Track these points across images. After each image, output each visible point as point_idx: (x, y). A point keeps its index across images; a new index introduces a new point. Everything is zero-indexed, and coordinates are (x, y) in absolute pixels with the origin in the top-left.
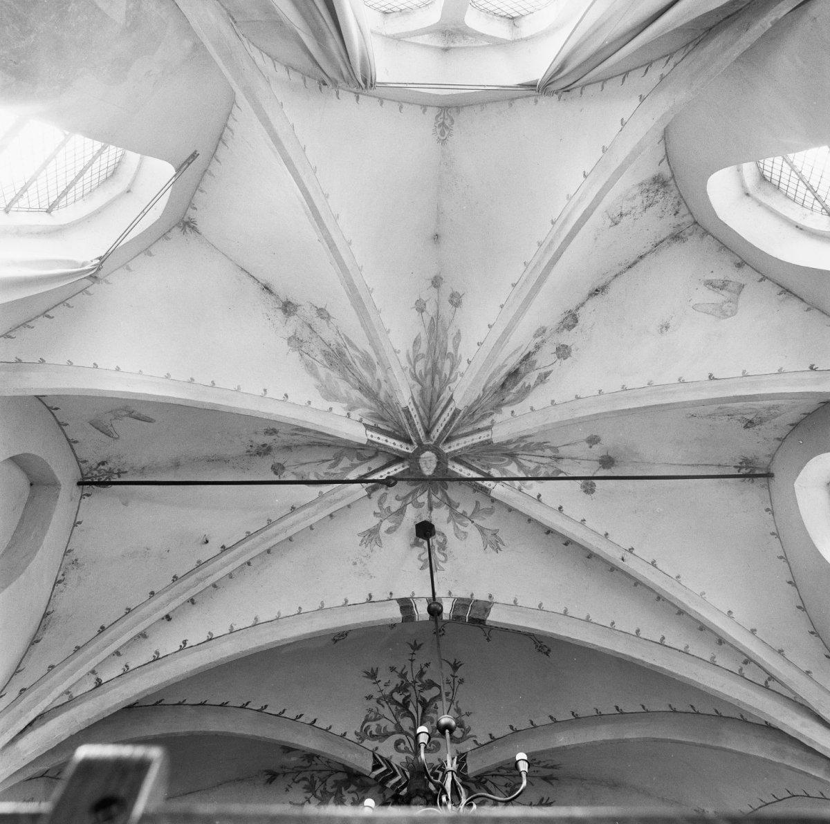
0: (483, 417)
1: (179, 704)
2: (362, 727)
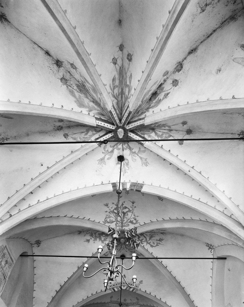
0: (142, 113)
1: (43, 218)
2: (105, 220)
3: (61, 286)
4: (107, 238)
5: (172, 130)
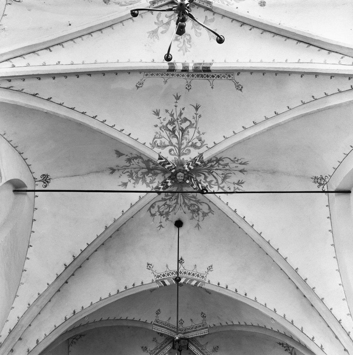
2: (153, 141)
3: (73, 256)
4: (155, 179)
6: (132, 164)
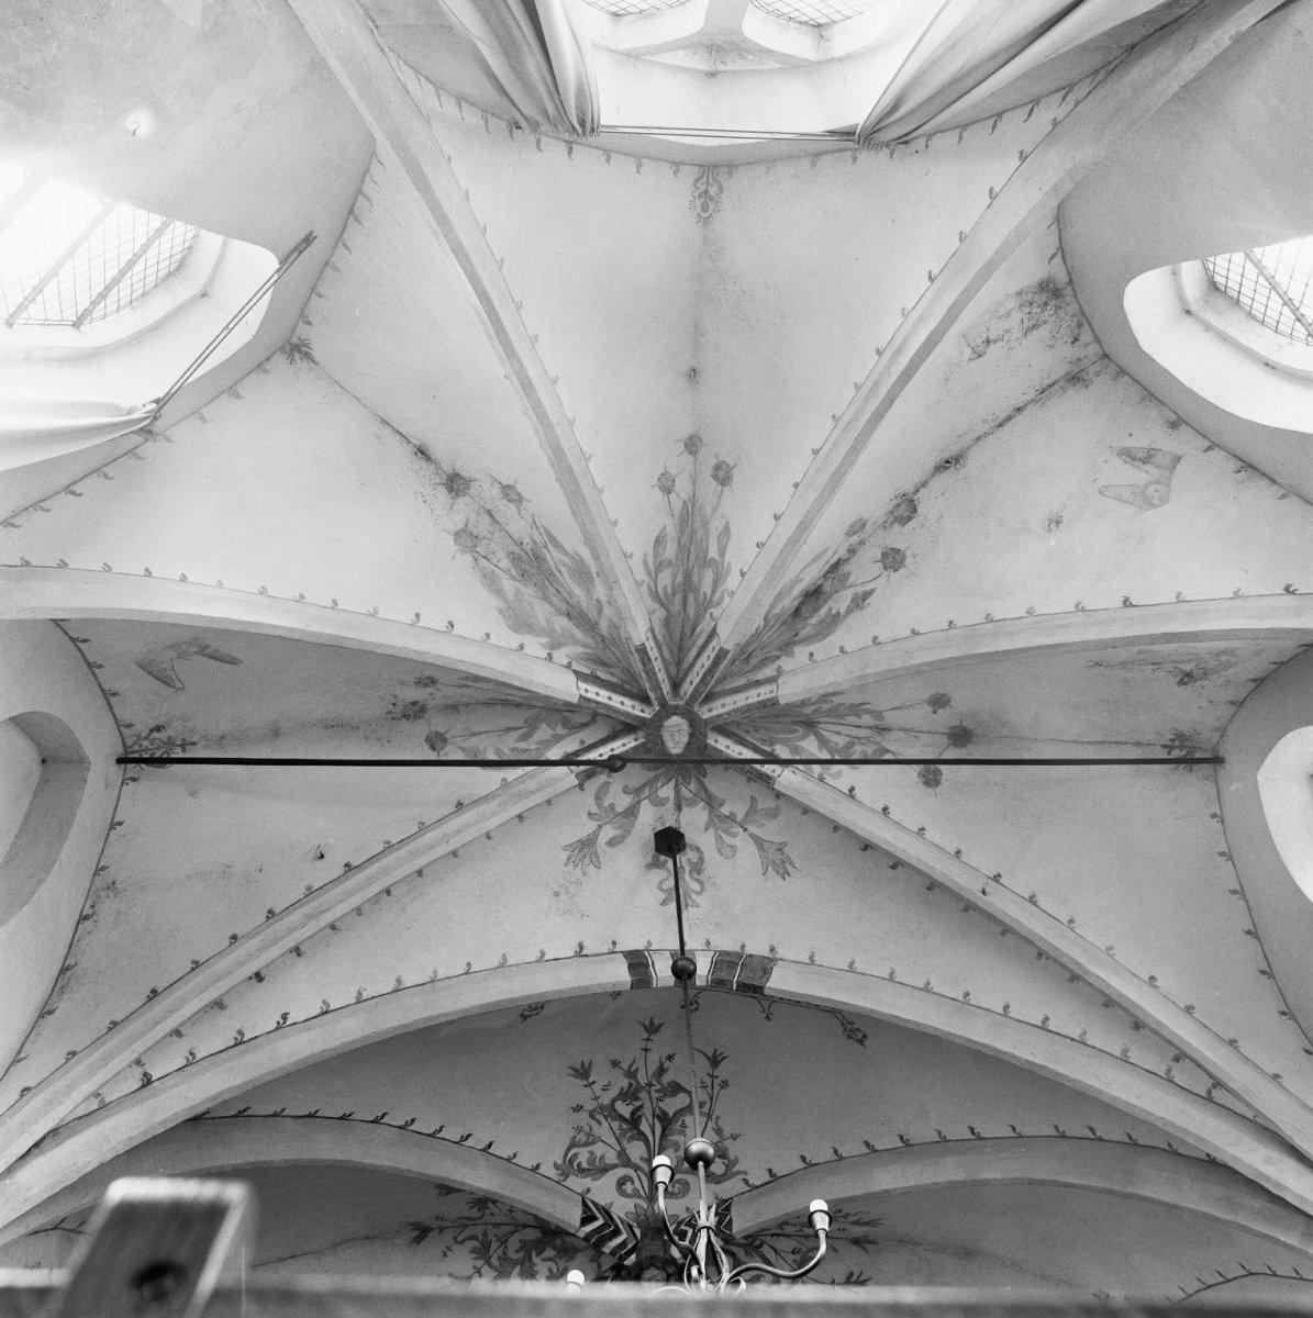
0: (764, 662)
2: (566, 1155)
5: (888, 729)
6: (487, 1212)
